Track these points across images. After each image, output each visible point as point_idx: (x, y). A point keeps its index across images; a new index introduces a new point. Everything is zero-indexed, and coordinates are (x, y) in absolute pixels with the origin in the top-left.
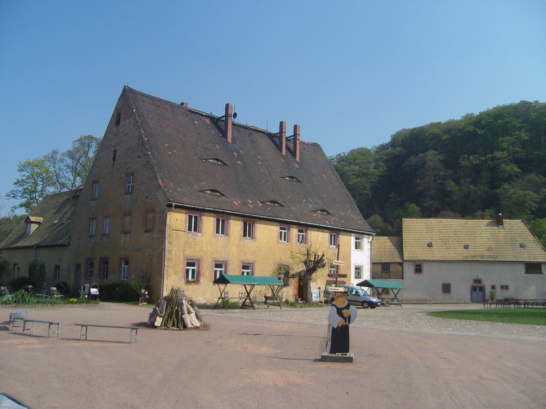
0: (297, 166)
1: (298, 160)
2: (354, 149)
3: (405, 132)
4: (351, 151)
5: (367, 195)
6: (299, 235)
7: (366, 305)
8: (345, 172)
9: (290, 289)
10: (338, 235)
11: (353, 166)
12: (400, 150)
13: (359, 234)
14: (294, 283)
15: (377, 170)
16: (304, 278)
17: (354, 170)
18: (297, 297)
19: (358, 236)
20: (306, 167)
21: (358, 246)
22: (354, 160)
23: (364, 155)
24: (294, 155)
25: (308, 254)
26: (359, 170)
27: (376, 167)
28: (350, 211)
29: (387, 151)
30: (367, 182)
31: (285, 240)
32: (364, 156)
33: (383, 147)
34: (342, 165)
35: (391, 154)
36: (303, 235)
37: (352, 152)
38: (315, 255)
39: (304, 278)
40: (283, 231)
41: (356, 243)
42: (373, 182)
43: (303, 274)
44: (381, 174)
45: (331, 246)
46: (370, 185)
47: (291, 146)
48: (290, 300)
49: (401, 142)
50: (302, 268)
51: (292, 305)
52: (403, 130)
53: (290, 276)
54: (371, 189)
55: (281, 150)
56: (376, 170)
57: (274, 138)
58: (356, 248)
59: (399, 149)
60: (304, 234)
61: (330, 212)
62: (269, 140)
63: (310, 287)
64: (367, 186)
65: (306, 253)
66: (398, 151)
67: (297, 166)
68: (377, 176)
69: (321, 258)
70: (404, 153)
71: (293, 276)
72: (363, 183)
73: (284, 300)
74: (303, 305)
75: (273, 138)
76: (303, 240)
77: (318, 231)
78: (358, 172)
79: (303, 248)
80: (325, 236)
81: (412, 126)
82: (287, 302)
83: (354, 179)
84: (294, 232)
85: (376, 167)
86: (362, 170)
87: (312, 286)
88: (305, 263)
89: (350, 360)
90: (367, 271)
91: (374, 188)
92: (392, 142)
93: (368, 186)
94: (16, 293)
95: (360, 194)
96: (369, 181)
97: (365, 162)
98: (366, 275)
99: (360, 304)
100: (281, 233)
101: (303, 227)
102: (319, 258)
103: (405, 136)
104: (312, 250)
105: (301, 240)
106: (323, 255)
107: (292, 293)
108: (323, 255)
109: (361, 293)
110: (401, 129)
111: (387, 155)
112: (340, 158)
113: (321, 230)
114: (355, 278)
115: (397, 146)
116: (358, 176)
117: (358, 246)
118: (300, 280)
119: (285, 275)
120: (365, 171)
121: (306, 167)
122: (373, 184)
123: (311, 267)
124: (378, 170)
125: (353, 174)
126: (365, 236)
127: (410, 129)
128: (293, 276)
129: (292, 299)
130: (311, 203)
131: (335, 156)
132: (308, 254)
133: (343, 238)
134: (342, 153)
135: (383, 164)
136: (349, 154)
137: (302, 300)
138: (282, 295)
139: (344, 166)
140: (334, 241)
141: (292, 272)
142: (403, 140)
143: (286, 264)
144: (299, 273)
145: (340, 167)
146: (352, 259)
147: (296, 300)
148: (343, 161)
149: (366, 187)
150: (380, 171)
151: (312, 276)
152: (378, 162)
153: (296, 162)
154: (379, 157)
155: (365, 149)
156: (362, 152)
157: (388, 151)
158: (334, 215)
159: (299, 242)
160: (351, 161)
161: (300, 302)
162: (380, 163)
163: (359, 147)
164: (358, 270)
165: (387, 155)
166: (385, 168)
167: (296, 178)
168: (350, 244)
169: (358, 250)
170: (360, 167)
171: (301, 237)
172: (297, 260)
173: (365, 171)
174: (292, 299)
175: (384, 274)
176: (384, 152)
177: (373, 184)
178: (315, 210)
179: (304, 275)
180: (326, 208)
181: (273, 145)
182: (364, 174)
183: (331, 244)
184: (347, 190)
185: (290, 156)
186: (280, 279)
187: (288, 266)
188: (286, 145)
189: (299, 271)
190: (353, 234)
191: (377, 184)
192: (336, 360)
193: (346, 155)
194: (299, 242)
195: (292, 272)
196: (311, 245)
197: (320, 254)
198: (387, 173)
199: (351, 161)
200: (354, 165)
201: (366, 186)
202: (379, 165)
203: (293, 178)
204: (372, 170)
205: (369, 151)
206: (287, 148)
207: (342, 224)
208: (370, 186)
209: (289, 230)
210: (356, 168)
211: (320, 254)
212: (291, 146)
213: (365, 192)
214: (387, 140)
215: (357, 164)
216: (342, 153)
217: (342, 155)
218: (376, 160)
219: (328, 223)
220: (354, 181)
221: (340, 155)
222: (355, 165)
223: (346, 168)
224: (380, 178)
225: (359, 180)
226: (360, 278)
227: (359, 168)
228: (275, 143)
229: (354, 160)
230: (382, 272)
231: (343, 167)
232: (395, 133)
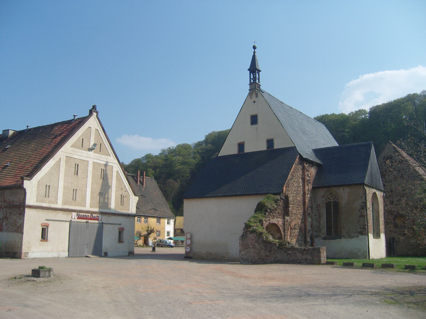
0: (144, 190)
1: (144, 187)
2: (180, 145)
3: (215, 134)
4: (178, 146)
5: (188, 177)
6: (145, 220)
7: (169, 246)
8: (174, 161)
9: (141, 241)
10: (160, 219)
11: (179, 157)
12: (210, 147)
13: (169, 218)
14: (142, 238)
15: (194, 160)
16: (147, 237)
17: (179, 160)
18: (144, 244)
19: (168, 219)
20: (148, 190)
21: (168, 223)
22: (179, 152)
23: (186, 149)
24: (143, 185)
25: (148, 228)
26: (182, 159)
27: (194, 158)
28: (165, 208)
29: (202, 147)
30: (187, 168)
31: (139, 222)
32: (186, 150)
33: (199, 144)
34: (171, 156)
35: (204, 149)
36: (146, 220)
37: (178, 146)
38: (151, 228)
39: (147, 237)
40: (139, 218)
41: (168, 222)
42: (192, 168)
43: (146, 235)
44: (197, 162)
45: (157, 223)
46: (190, 170)
47: (142, 180)
48: (141, 245)
49: (212, 141)
50: (146, 233)
51: (142, 247)
52: (213, 132)
53: (141, 236)
54: (190, 173)
55: (137, 183)
56: (194, 160)
57: (134, 177)
58: (168, 224)
59: (209, 145)
60: (146, 219)
61: (157, 209)
62: (132, 179)
63: (149, 240)
64: (188, 171)
65: (147, 227)
66: (209, 147)
67: (144, 190)
68: (194, 164)
69: (153, 229)
70: (213, 149)
71: (142, 236)
72: (185, 169)
73: (139, 245)
74: (146, 246)
75: (134, 177)
76: (147, 222)
77: (152, 218)
78: (182, 161)
79: (146, 225)
80: (154, 220)
81: (220, 130)
82: (140, 246)
83: (179, 166)
84: (143, 219)
85: (194, 158)
86: (184, 160)
87: (149, 239)
88: (147, 231)
89: (155, 252)
90: (172, 233)
91: (193, 173)
92: (206, 141)
93: (188, 171)
94: (310, 243)
95: (183, 176)
96: (189, 167)
97: (187, 154)
98: (172, 235)
99: (167, 246)
100: (138, 219)
101: (146, 217)
102: (152, 229)
103: (215, 136)
104: (150, 226)
105: (145, 221)
106: (154, 228)
107: (142, 242)
108: (154, 228)
109: (168, 242)
110: (212, 132)
111: (201, 150)
112: (170, 150)
113: (153, 217)
114: (167, 236)
115: (209, 143)
116: (182, 164)
117: (168, 223)
118: (145, 238)
119: (140, 235)
120: (186, 160)
121: (148, 190)
122: (191, 169)
123: (149, 233)
124: (195, 160)
125: (179, 163)
126: (172, 219)
127: (218, 131)
128: (142, 236)
129: (142, 245)
130: (149, 206)
131: (167, 148)
132: (148, 228)
133: (162, 220)
134: (172, 147)
135: (198, 156)
136: (176, 148)
137: (145, 245)
138: (138, 243)
139: (173, 156)
140: (159, 222)
141: (142, 235)
142: (213, 139)
143: (140, 231)
144: (145, 234)
145: (169, 157)
146: (166, 228)
147: (143, 245)
148: (172, 153)
149: (187, 172)
150: (196, 161)
151: (150, 236)
152: (195, 154)
153: (144, 188)
154: (196, 151)
155: (187, 144)
156: (184, 147)
157: (202, 147)
158: (159, 211)
159: (144, 222)
160: (177, 153)
161: (145, 245)
162: (197, 155)
163: (184, 143)
164: (168, 233)
165: (201, 150)
166: (200, 159)
167: (143, 196)
168: (165, 222)
169: (169, 224)
170: (183, 158)
171: (145, 220)
172: (144, 230)
173: (186, 160)
174: (142, 245)
175: (181, 234)
176: (200, 147)
177: (191, 169)
178: (151, 209)
179: (147, 235)
180: (155, 208)
181: (134, 180)
182: (185, 162)
183: (157, 223)
184: (165, 199)
185: (141, 185)
186: (137, 237)
187: (140, 232)
188: (139, 180)
189: (145, 234)
190: (166, 218)
191: (194, 169)
192: (153, 252)
193: (175, 148)
194: (144, 222)
195: (142, 235)
196: (149, 224)
197: (152, 228)
198: (201, 162)
199: (177, 153)
200: (179, 156)
201: (187, 171)
202: (196, 156)
203: (142, 195)
204: (191, 160)
205: (190, 145)
206: (140, 181)
207: (162, 215)
208: (190, 171)
209: (141, 218)
210: (181, 158)
211: (152, 228)
212: (142, 180)
213: (186, 175)
214: (202, 138)
215: (181, 156)
216: (172, 147)
217: (171, 148)
218: (195, 153)
219: (156, 214)
220: (179, 167)
221: (170, 148)
222: (180, 156)
223: (174, 158)
224: (196, 165)
225: (182, 166)
226: (169, 236)
227: (182, 158)
228: (135, 180)
229: (179, 152)
230: (181, 233)
231: (172, 157)
232: (208, 135)
